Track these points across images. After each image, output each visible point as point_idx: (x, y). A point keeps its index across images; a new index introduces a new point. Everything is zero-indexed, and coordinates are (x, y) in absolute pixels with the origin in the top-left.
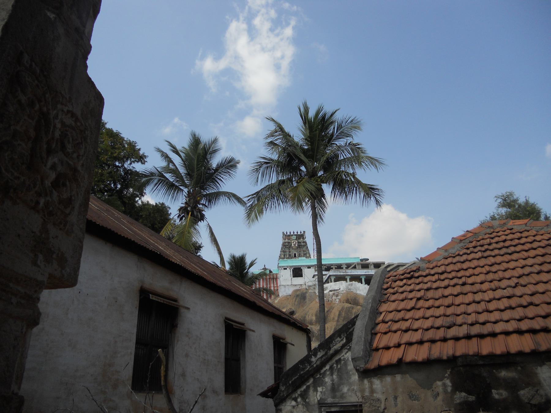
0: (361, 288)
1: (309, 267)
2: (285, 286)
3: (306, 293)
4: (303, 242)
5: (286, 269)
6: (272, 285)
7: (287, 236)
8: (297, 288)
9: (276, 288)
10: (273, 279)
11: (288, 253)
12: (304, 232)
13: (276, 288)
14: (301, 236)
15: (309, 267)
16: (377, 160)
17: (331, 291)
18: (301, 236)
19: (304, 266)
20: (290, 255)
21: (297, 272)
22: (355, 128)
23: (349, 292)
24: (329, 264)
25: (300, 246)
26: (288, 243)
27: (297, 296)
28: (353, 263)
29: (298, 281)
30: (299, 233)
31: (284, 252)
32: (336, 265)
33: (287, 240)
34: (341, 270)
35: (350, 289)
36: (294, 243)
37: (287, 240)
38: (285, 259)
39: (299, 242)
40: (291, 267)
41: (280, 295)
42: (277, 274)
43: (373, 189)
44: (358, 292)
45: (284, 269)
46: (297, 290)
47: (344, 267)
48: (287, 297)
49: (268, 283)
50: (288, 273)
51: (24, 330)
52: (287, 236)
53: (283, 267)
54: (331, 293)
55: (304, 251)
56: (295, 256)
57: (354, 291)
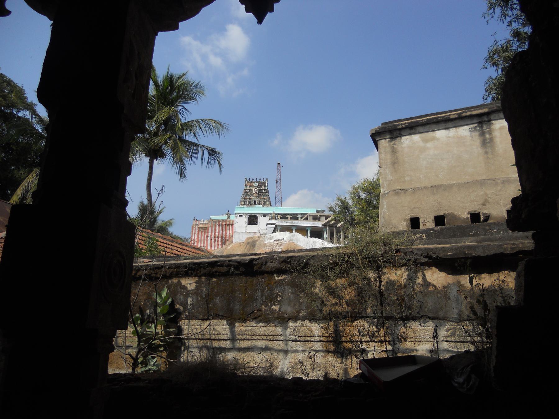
0: (301, 240)
1: (264, 215)
2: (239, 233)
3: (257, 240)
4: (265, 190)
5: (242, 216)
6: (228, 231)
7: (249, 182)
8: (251, 235)
9: (231, 235)
10: (229, 225)
11: (248, 200)
12: (267, 180)
13: (231, 235)
14: (262, 184)
15: (264, 215)
16: (221, 125)
17: (275, 240)
18: (262, 184)
19: (259, 214)
20: (250, 202)
21: (252, 220)
22: (200, 92)
23: (291, 242)
24: (284, 214)
25: (260, 193)
26: (250, 190)
27: (248, 243)
28: (305, 214)
29: (253, 228)
30: (262, 181)
31: (244, 199)
32: (291, 214)
33: (248, 187)
34: (287, 221)
35: (292, 240)
36: (255, 190)
37: (248, 187)
38: (245, 206)
39: (260, 190)
40: (246, 214)
41: (234, 242)
42: (233, 221)
43: (215, 152)
44: (299, 243)
45: (240, 216)
46: (251, 238)
47: (299, 217)
48: (239, 245)
49: (224, 229)
50: (244, 219)
51: (169, 238)
52: (249, 182)
53: (238, 213)
54: (276, 242)
55: (264, 199)
56: (255, 204)
57: (296, 242)
